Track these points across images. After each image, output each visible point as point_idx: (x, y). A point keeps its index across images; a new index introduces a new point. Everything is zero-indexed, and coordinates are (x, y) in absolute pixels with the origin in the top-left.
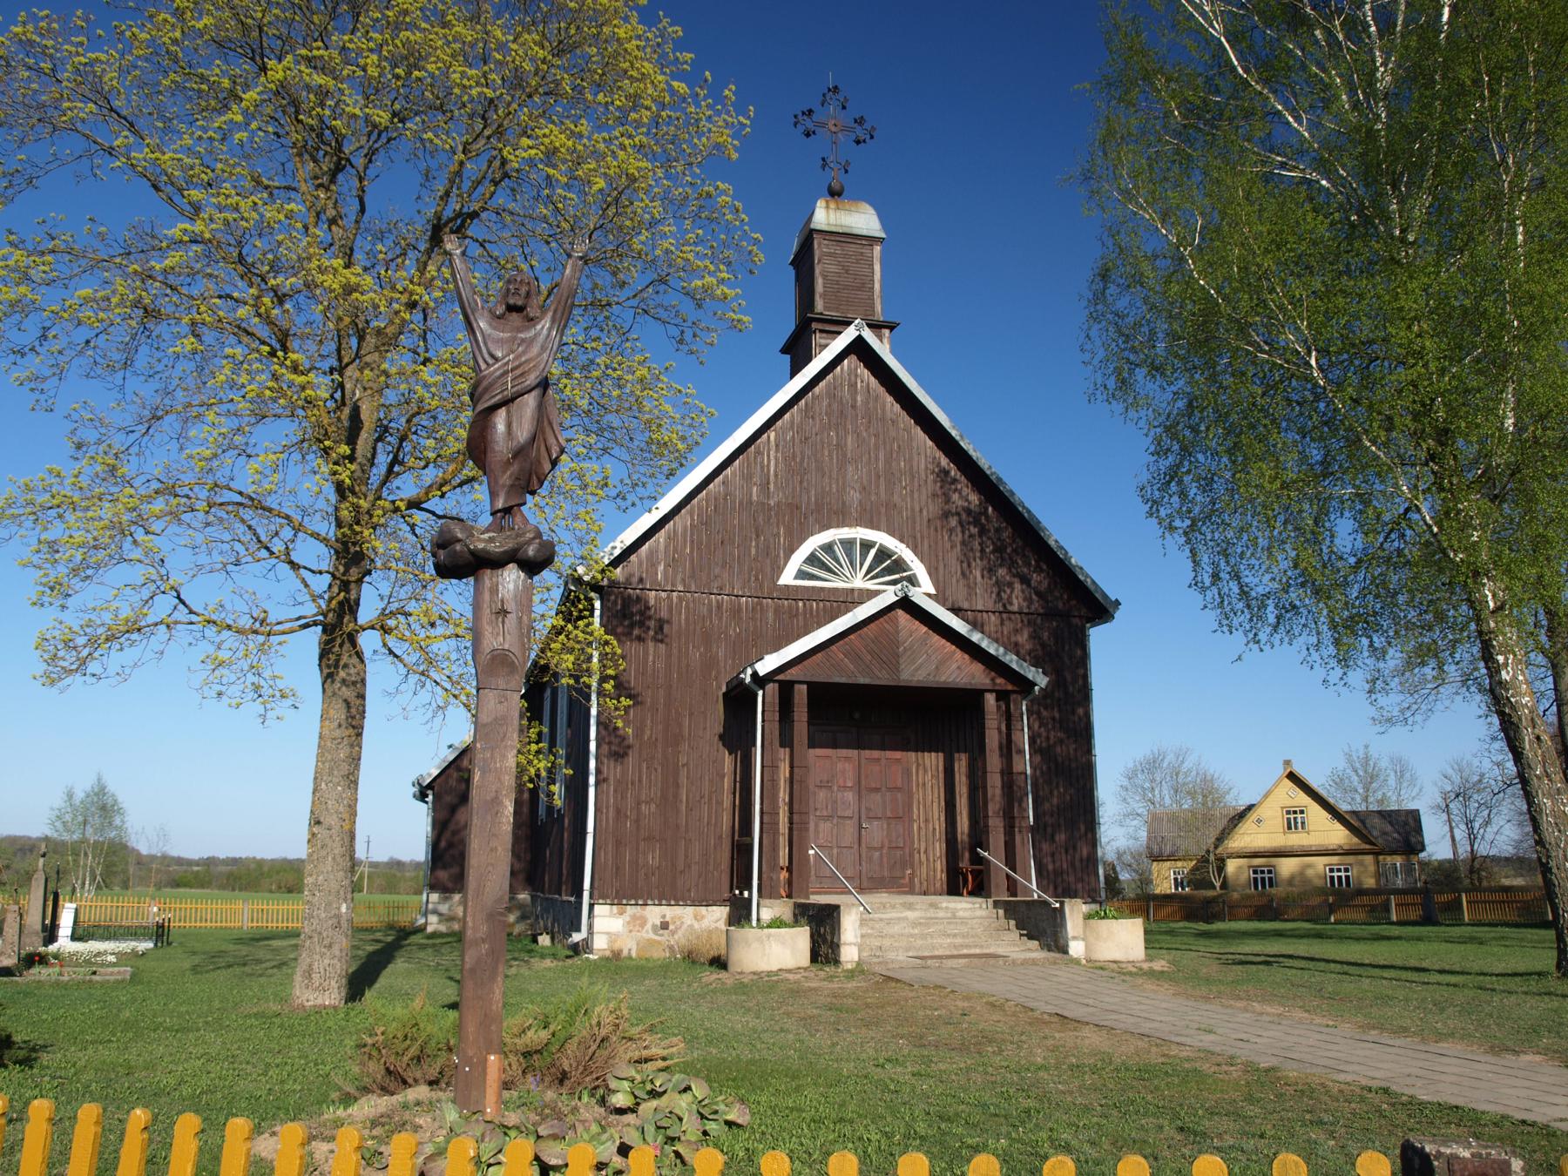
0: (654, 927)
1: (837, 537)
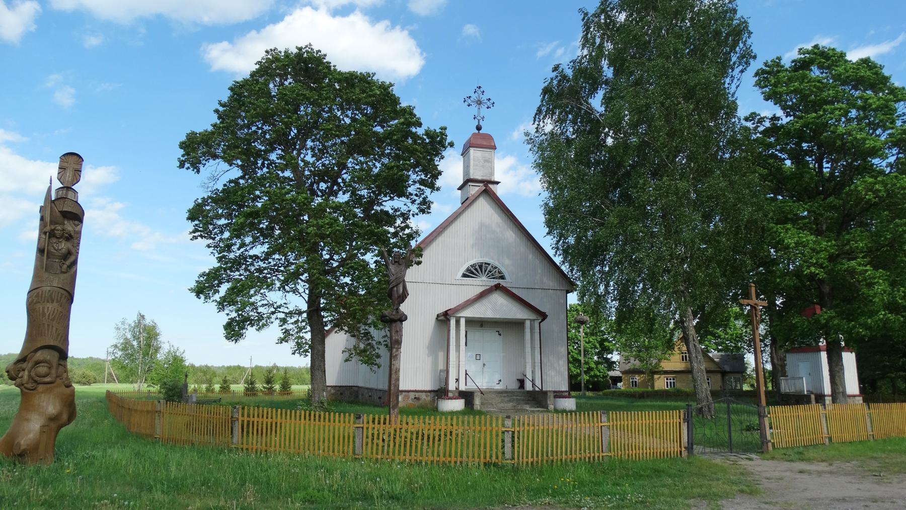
0: (412, 399)
1: (469, 265)
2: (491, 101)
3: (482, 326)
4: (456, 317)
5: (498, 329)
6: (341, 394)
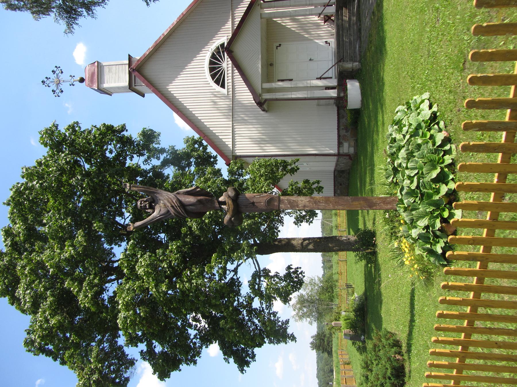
2: (55, 69)
3: (271, 65)
4: (263, 92)
5: (275, 47)
6: (341, 185)
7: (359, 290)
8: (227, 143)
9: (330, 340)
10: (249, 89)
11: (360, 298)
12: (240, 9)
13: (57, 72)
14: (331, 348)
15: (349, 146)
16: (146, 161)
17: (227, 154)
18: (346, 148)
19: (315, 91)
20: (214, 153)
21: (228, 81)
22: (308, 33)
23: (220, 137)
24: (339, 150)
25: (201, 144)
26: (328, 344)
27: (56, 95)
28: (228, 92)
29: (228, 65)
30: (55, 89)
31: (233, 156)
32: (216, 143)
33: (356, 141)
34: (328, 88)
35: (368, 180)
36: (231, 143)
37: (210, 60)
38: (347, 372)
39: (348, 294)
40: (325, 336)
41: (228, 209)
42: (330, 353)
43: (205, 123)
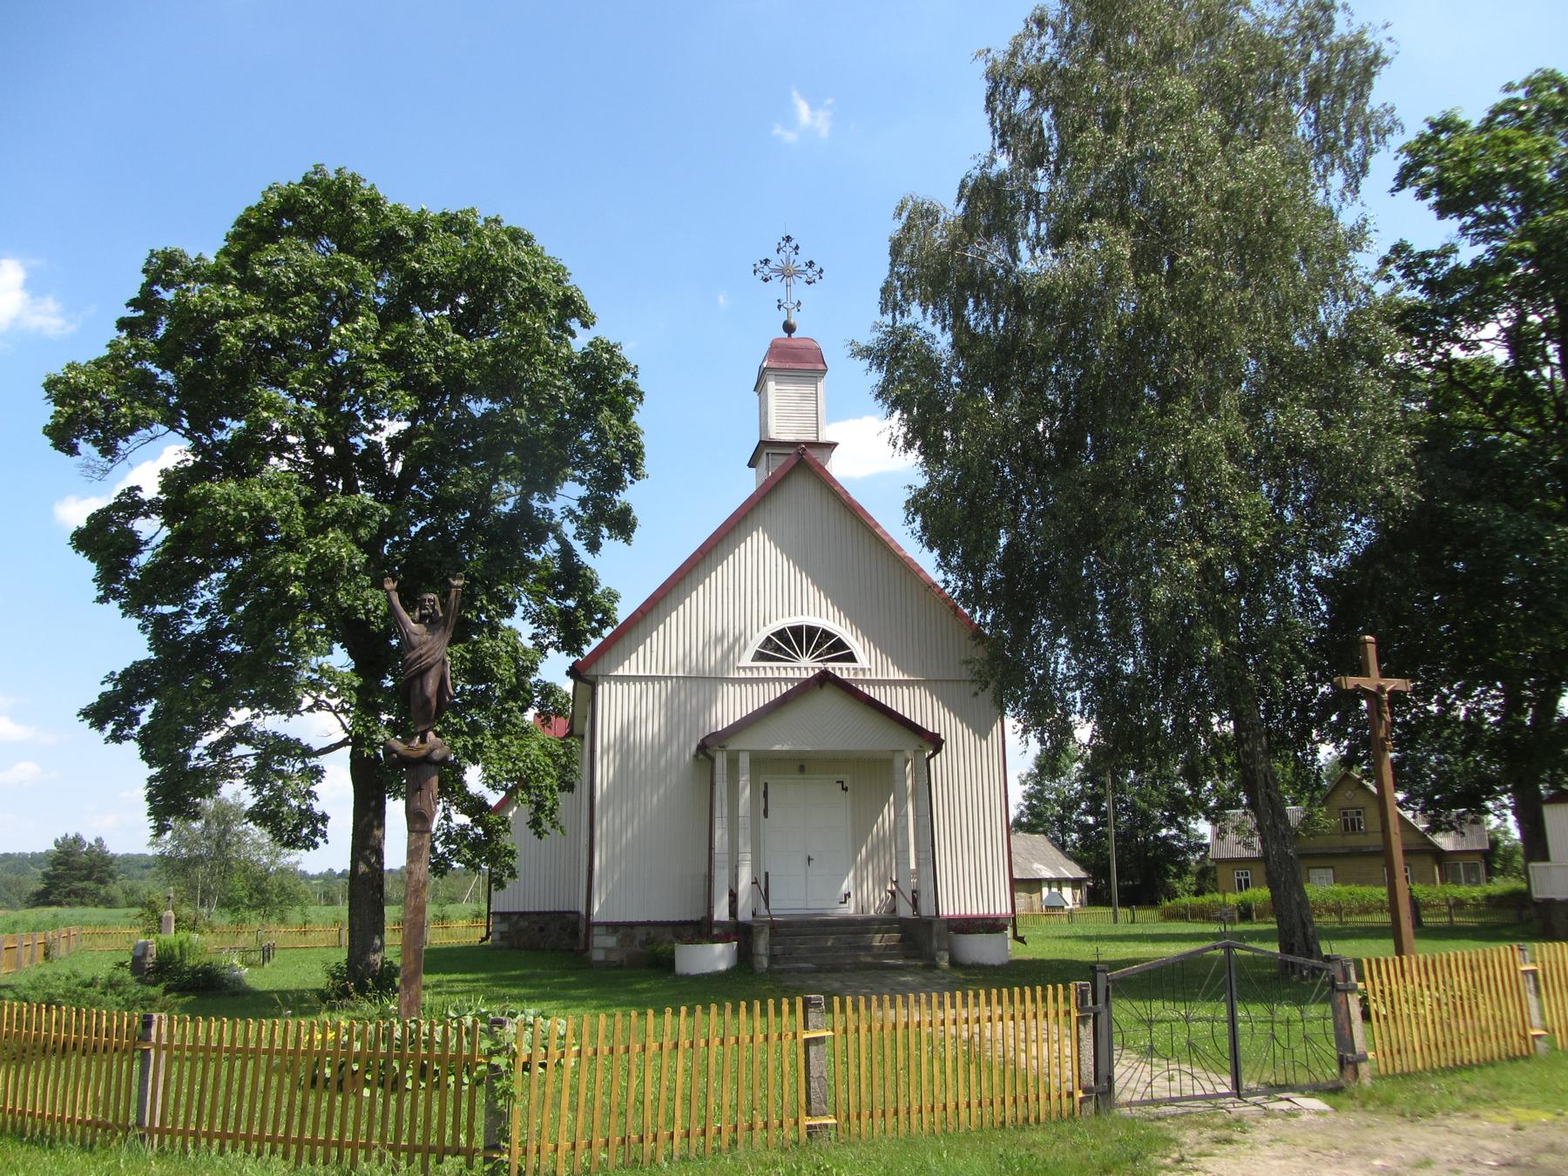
2: (817, 268)
3: (802, 769)
5: (841, 777)
6: (541, 929)
7: (257, 979)
8: (627, 663)
9: (86, 900)
10: (748, 716)
11: (238, 981)
12: (929, 699)
13: (810, 272)
14: (59, 904)
15: (608, 950)
16: (571, 512)
17: (600, 662)
18: (603, 945)
19: (726, 871)
20: (587, 650)
21: (770, 669)
22: (870, 857)
23: (641, 649)
24: (600, 924)
25: (603, 624)
26: (75, 893)
27: (759, 265)
28: (744, 668)
29: (806, 669)
30: (772, 265)
31: (597, 676)
32: (607, 655)
33: (620, 966)
34: (733, 896)
35: (515, 991)
36: (627, 673)
37: (818, 629)
38: (29, 950)
39: (245, 951)
40: (101, 881)
41: (412, 749)
42: (42, 899)
43: (674, 614)
